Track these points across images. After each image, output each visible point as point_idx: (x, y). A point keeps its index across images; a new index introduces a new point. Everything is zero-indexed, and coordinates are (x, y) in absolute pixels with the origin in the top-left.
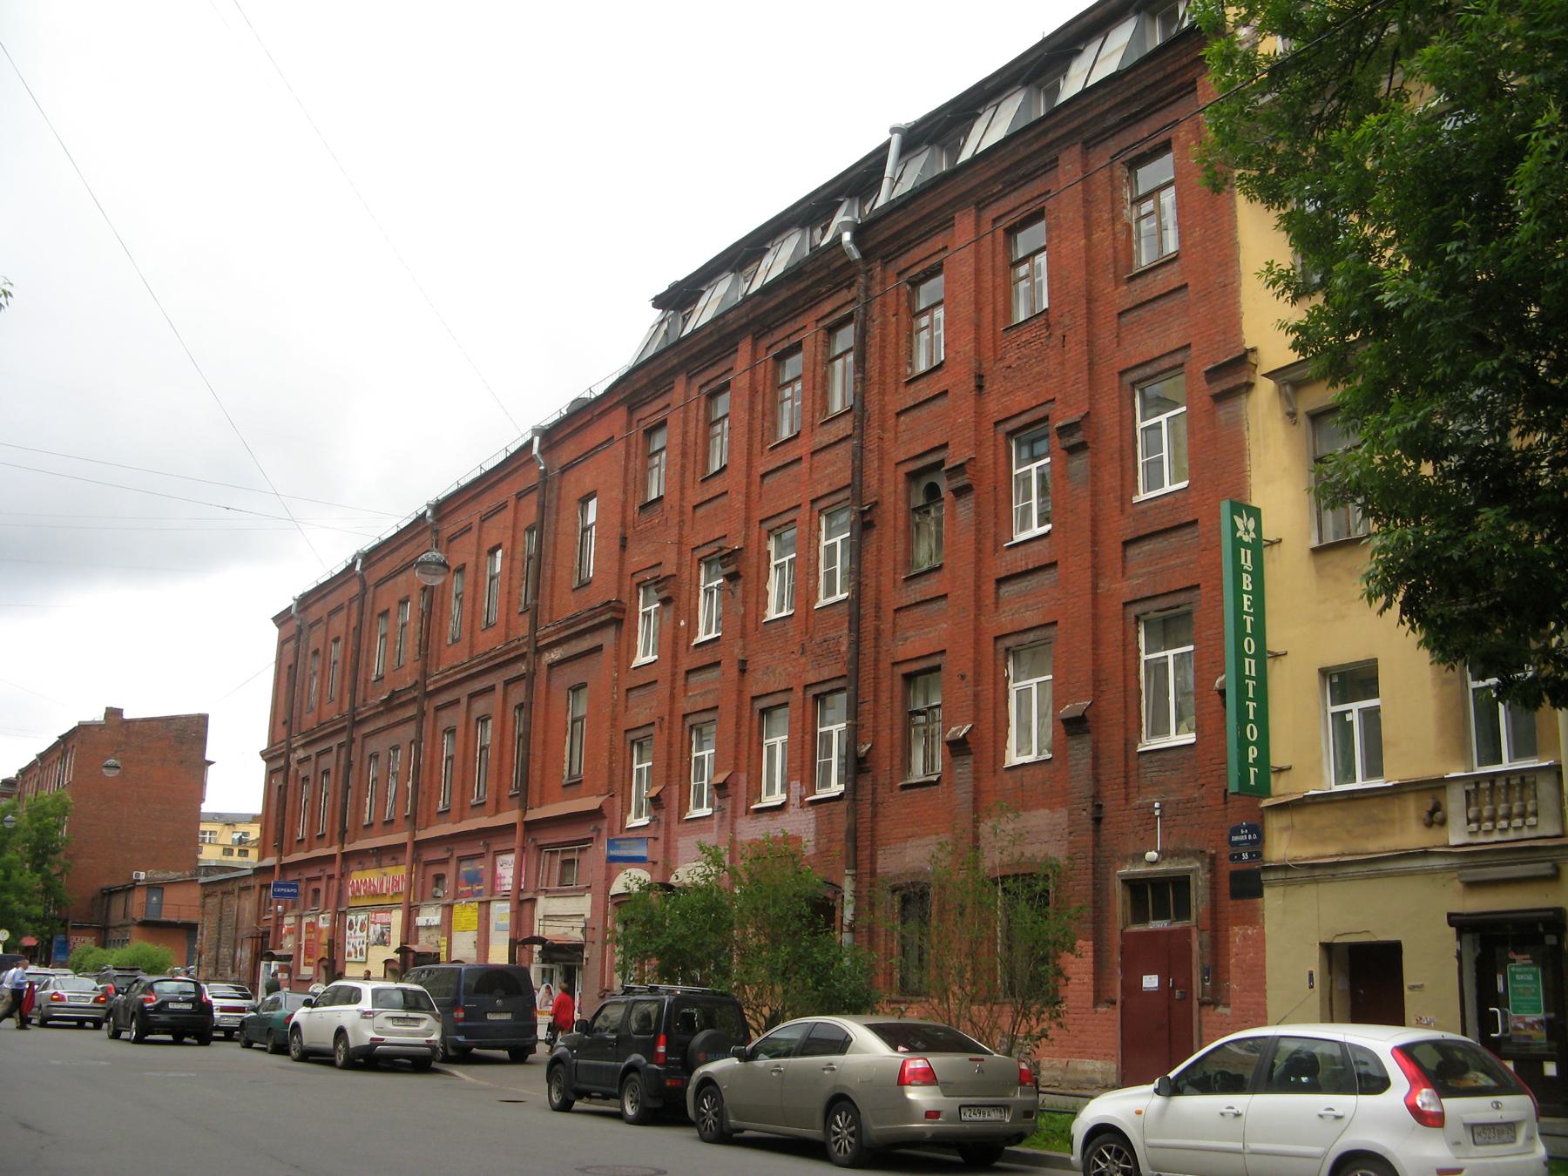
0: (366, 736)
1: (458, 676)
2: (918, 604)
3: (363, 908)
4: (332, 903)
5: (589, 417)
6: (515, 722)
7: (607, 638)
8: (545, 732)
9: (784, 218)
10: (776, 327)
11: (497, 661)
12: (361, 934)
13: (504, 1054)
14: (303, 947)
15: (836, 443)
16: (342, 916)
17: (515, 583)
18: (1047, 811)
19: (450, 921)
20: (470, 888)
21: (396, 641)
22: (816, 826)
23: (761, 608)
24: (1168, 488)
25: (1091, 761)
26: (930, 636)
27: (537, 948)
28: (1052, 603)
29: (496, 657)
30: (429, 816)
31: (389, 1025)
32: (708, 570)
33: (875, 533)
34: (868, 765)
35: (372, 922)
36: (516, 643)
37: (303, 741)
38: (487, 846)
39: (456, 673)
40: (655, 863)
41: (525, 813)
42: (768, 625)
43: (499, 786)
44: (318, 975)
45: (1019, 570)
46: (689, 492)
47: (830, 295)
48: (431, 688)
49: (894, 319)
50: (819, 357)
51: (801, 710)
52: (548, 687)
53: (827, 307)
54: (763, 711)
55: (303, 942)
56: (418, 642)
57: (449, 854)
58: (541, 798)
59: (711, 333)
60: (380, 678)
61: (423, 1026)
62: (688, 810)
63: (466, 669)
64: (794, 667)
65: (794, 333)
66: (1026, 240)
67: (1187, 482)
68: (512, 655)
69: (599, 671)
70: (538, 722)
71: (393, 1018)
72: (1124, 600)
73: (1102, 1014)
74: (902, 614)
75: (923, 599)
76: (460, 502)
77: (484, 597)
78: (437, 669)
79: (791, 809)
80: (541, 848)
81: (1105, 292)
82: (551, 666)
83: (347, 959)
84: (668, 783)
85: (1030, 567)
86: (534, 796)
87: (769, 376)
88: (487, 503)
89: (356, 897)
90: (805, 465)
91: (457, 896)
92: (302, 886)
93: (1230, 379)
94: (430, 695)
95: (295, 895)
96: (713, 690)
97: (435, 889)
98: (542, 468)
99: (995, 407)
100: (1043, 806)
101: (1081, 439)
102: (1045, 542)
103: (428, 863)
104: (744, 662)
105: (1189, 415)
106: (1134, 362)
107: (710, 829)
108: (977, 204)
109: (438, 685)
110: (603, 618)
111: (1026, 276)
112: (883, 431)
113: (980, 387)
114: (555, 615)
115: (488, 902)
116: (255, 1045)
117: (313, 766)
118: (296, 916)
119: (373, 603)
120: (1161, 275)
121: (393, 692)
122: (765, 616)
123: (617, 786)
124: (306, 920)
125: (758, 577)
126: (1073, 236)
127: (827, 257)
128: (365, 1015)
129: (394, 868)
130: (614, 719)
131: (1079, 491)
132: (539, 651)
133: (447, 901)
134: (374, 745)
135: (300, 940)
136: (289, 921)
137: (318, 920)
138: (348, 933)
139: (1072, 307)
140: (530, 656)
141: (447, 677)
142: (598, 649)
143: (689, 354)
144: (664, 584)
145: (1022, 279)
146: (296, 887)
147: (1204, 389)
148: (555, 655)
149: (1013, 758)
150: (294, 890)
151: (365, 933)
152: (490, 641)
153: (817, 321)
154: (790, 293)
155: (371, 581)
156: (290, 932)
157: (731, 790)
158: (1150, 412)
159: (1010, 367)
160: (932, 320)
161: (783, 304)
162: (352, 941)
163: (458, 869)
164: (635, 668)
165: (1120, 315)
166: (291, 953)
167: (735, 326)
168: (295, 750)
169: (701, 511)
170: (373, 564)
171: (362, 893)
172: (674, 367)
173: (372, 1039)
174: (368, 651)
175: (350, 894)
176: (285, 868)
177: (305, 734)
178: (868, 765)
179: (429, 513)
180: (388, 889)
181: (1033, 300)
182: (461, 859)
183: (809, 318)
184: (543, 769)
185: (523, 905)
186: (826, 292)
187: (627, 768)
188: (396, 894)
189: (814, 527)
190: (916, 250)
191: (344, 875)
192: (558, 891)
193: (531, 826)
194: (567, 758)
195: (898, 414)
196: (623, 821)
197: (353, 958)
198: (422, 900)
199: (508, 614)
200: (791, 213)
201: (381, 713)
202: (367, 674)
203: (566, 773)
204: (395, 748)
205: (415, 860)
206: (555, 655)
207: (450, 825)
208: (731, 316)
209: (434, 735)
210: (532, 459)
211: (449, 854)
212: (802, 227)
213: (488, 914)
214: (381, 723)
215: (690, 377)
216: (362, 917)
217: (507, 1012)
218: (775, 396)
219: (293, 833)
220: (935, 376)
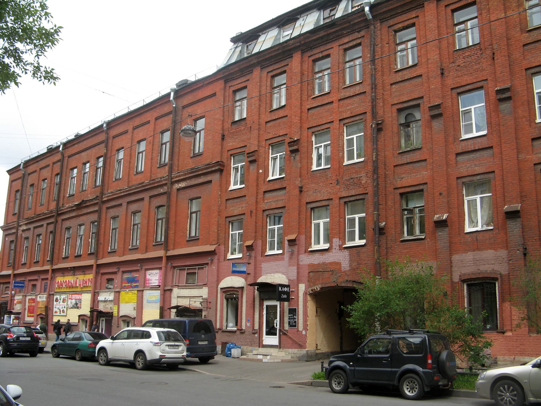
0: (63, 220)
1: (122, 194)
2: (408, 163)
3: (64, 293)
4: (47, 291)
5: (202, 84)
6: (155, 214)
7: (215, 177)
8: (176, 218)
9: (309, 6)
10: (314, 48)
11: (146, 187)
12: (63, 304)
13: (197, 360)
14: (27, 309)
15: (353, 96)
16: (52, 296)
17: (154, 155)
18: (493, 251)
19: (119, 298)
20: (130, 284)
21: (81, 180)
22: (350, 258)
23: (309, 164)
24: (356, 160)
25: (521, 229)
26: (416, 177)
27: (174, 311)
28: (491, 163)
29: (199, 171)
30: (103, 253)
31: (167, 349)
32: (272, 150)
33: (382, 133)
34: (384, 231)
35: (70, 299)
36: (159, 179)
37: (26, 222)
38: (141, 266)
39: (121, 193)
40: (249, 274)
41: (166, 253)
42: (314, 172)
43: (147, 241)
44: (37, 321)
45: (470, 150)
46: (262, 116)
47: (348, 34)
48: (105, 199)
49: (387, 45)
50: (341, 61)
51: (338, 208)
52: (177, 198)
53: (346, 40)
54: (312, 209)
55: (27, 307)
56: (94, 180)
57: (118, 270)
58: (174, 246)
59: (278, 50)
60: (71, 196)
61: (181, 348)
62: (266, 251)
63: (127, 191)
64: (332, 190)
65: (326, 50)
66: (350, 55)
67: (363, 159)
68: (156, 185)
69: (213, 190)
70: (173, 213)
71: (168, 345)
72: (534, 163)
73: (534, 337)
74: (398, 168)
75: (411, 161)
76: (121, 121)
77: (135, 161)
78: (108, 191)
79: (334, 250)
80: (174, 267)
81: (515, 36)
82: (178, 190)
83: (54, 314)
84: (255, 240)
85: (477, 148)
86: (171, 246)
87: (311, 68)
88: (137, 121)
89: (59, 288)
90: (335, 105)
91: (122, 288)
92: (26, 283)
93: (436, 111)
94: (104, 202)
95: (23, 287)
96: (282, 200)
97: (107, 285)
98: (174, 106)
99: (450, 82)
100: (490, 249)
101: (510, 95)
102: (485, 138)
103: (103, 274)
104: (302, 187)
105: (365, 135)
106: (534, 65)
107: (283, 259)
108: (302, 51)
109: (110, 198)
110: (213, 169)
111: (239, 106)
112: (384, 91)
113: (442, 74)
114: (180, 168)
115: (143, 291)
116: (61, 356)
117: (32, 233)
118: (23, 296)
119: (67, 164)
120: (405, 72)
121: (83, 201)
122: (311, 168)
123: (222, 241)
124: (28, 298)
125: (307, 152)
126: (497, 12)
127: (350, 18)
128: (156, 344)
129: (62, 277)
130: (219, 212)
131: (507, 117)
132: (173, 183)
133: (117, 290)
134: (67, 224)
135: (25, 306)
136: (18, 298)
137: (37, 298)
138: (55, 303)
139: (497, 42)
140: (169, 185)
141: (115, 194)
142: (210, 182)
143: (264, 58)
144: (253, 154)
145: (238, 106)
146: (23, 283)
147: (493, 96)
148: (182, 185)
149: (468, 229)
150: (23, 285)
151: (66, 304)
152: (136, 180)
153: (339, 46)
154: (326, 33)
155: (66, 155)
156: (19, 302)
157: (297, 242)
158: (318, 142)
159: (459, 66)
160: (242, 103)
161: (322, 38)
162: (57, 307)
163: (122, 276)
164: (270, 181)
165: (524, 45)
166: (20, 311)
167: (292, 47)
168: (21, 226)
169: (269, 125)
170: (68, 148)
171: (64, 286)
172: (254, 64)
173: (160, 356)
174: (65, 184)
175: (56, 286)
176: (15, 276)
177: (27, 219)
178: (384, 231)
179: (105, 125)
180: (80, 285)
181: (241, 113)
182: (124, 272)
183: (335, 45)
184: (175, 233)
185: (166, 292)
186: (346, 33)
187: (227, 233)
188: (84, 287)
189: (341, 131)
190: (400, 17)
191: (53, 278)
192: (185, 286)
193: (169, 258)
194: (188, 229)
195: (392, 84)
196: (226, 256)
197: (58, 314)
198: (100, 289)
199: (151, 168)
200: (313, 4)
201: (74, 210)
202: (64, 193)
203: (188, 235)
204: (80, 225)
205: (97, 273)
206: (182, 185)
207: (26, 269)
208: (291, 42)
209: (106, 219)
210: (169, 101)
211: (118, 270)
212: (319, 10)
213: (142, 296)
214: (73, 214)
215: (262, 68)
216: (63, 296)
217: (206, 341)
218: (313, 76)
219: (20, 260)
220: (414, 69)
